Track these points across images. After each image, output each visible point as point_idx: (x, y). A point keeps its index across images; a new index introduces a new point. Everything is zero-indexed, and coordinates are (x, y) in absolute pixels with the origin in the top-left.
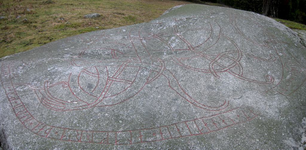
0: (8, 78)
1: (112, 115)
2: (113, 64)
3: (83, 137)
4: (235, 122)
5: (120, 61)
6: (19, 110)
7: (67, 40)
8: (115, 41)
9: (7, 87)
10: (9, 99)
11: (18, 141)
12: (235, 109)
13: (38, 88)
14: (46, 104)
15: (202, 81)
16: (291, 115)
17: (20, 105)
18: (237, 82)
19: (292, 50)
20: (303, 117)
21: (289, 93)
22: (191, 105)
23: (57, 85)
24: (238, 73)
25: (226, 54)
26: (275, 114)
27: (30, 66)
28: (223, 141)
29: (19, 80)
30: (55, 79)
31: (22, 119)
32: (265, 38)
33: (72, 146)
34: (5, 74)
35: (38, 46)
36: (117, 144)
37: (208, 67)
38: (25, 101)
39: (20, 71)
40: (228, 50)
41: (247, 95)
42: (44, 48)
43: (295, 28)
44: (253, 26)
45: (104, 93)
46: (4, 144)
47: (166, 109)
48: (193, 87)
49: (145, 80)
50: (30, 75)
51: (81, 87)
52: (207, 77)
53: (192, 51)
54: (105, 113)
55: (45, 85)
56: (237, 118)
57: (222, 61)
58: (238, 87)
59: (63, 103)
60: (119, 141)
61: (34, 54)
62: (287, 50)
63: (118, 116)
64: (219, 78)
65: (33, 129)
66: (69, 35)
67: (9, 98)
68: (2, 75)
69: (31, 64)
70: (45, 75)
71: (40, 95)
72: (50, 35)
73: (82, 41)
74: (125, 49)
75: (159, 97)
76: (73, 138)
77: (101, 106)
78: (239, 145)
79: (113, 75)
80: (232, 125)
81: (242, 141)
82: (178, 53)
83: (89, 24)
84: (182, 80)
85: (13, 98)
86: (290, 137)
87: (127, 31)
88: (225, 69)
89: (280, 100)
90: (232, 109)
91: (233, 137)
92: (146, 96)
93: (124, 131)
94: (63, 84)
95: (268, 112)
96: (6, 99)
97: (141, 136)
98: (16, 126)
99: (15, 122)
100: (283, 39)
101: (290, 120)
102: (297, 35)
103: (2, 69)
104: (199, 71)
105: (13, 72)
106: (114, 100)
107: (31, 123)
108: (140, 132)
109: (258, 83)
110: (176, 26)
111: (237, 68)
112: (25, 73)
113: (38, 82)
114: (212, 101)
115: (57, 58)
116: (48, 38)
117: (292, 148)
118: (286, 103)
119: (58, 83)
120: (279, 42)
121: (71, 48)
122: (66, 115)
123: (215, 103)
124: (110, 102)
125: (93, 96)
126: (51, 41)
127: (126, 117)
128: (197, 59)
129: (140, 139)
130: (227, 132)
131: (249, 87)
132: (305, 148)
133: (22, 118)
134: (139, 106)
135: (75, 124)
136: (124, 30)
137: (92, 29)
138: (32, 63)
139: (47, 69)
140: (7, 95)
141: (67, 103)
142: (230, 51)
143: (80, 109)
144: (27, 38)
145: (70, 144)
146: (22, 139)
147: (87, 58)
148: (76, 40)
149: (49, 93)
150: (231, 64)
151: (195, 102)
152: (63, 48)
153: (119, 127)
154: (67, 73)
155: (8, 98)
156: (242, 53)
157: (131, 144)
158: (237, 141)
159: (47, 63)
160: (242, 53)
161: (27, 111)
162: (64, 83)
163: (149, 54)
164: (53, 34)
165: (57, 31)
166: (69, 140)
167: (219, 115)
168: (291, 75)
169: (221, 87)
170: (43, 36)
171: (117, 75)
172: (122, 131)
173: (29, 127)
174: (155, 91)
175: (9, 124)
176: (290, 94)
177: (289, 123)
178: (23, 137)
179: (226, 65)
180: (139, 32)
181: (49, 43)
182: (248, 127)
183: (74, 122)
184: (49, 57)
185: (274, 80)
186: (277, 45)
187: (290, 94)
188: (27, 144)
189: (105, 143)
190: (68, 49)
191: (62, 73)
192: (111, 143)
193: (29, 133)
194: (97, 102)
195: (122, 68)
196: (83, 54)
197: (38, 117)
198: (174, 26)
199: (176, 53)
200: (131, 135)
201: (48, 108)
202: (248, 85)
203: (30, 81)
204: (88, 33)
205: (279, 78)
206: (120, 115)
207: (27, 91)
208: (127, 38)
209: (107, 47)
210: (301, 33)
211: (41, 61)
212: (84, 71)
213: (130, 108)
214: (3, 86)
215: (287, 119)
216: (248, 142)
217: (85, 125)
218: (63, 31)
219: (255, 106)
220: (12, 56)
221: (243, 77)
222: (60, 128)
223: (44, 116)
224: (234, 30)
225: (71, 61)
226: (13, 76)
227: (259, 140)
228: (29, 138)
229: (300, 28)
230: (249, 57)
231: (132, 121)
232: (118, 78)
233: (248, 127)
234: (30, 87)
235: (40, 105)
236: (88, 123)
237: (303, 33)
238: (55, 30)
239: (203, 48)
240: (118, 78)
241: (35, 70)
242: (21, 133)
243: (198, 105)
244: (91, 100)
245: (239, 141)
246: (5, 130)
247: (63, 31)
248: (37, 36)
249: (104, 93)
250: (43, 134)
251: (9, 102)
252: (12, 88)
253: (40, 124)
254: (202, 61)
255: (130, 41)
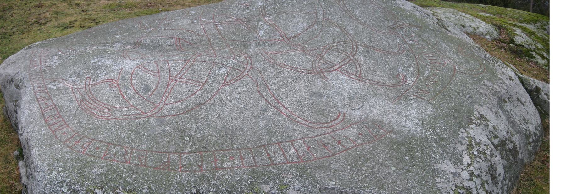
0: (38, 71)
1: (176, 129)
2: (176, 57)
3: (133, 158)
4: (357, 142)
5: (187, 53)
6: (50, 114)
7: (119, 25)
8: (180, 27)
9: (36, 83)
10: (37, 99)
11: (45, 155)
12: (355, 123)
13: (77, 86)
14: (86, 108)
15: (302, 86)
16: (440, 127)
17: (51, 107)
18: (353, 85)
19: (427, 35)
20: (460, 128)
21: (432, 95)
22: (287, 119)
23: (103, 83)
24: (355, 73)
25: (334, 46)
26: (415, 128)
27: (68, 56)
28: (342, 172)
29: (53, 74)
30: (100, 75)
31: (52, 126)
32: (389, 23)
33: (117, 169)
34: (34, 65)
35: (80, 30)
36: (183, 171)
37: (310, 66)
38: (59, 102)
39: (55, 62)
40: (336, 41)
41: (370, 103)
42: (89, 33)
43: (427, 6)
44: (369, 7)
45: (164, 98)
46: (28, 158)
47: (250, 125)
48: (289, 93)
49: (221, 80)
50: (67, 68)
51: (134, 89)
52: (309, 80)
53: (286, 43)
54: (165, 127)
55: (87, 83)
56: (359, 138)
57: (329, 57)
58: (356, 93)
59: (108, 109)
60: (185, 167)
61: (74, 40)
62: (419, 36)
63: (183, 131)
64: (327, 81)
65: (66, 141)
66: (122, 18)
67: (38, 97)
68: (31, 66)
69: (70, 54)
70: (88, 69)
71: (78, 95)
72: (96, 16)
73: (139, 26)
74: (194, 38)
75: (242, 106)
76: (119, 158)
77: (161, 117)
78: (366, 177)
79: (177, 73)
80: (353, 147)
81: (371, 171)
82: (266, 44)
83: (149, 5)
84: (273, 83)
85: (43, 98)
86: (445, 159)
87: (196, 13)
88: (334, 68)
89: (419, 106)
90: (350, 125)
91: (355, 165)
92: (223, 104)
93: (192, 153)
94: (110, 82)
95: (405, 126)
96: (33, 99)
97: (216, 160)
98: (44, 135)
99: (43, 130)
100: (411, 21)
101: (440, 134)
102: (431, 15)
103: (31, 58)
104: (297, 71)
105: (45, 63)
106: (177, 108)
107: (65, 133)
108: (214, 154)
109: (386, 86)
110: (263, 7)
111: (352, 66)
112: (60, 66)
113: (77, 78)
114: (321, 114)
115: (104, 48)
116: (94, 20)
117: (451, 175)
118: (430, 110)
119: (104, 81)
120: (405, 26)
121: (124, 34)
122: (112, 125)
123: (325, 116)
124: (173, 110)
125: (150, 102)
126: (97, 25)
127: (195, 132)
128: (294, 54)
129: (214, 165)
130: (347, 159)
131: (373, 91)
132: (470, 172)
133: (52, 125)
134: (213, 117)
135: (124, 139)
136: (193, 13)
137: (152, 12)
138: (71, 51)
139: (90, 61)
140: (35, 93)
141: (114, 109)
142: (339, 42)
143: (131, 119)
144: (66, 19)
145: (115, 166)
146: (51, 153)
147: (145, 49)
148: (130, 24)
149: (91, 93)
150: (343, 59)
151: (293, 115)
152: (113, 35)
153: (184, 147)
154: (116, 68)
155: (37, 97)
156: (356, 44)
157: (202, 171)
158: (363, 170)
159: (91, 53)
160: (356, 44)
161: (60, 116)
162: (112, 81)
163: (228, 44)
164: (100, 15)
165: (107, 12)
166: (114, 160)
167: (332, 134)
168: (431, 71)
169: (330, 93)
170: (87, 17)
171: (182, 74)
172: (189, 152)
173: (61, 138)
174: (236, 97)
175: (35, 132)
176: (434, 97)
177: (440, 138)
178: (52, 150)
179: (335, 61)
180: (213, 15)
181: (94, 27)
182: (378, 149)
183: (122, 136)
184: (94, 45)
185: (406, 79)
186: (404, 30)
187: (434, 97)
188: (57, 160)
189: (165, 169)
190: (120, 36)
191: (110, 67)
192: (173, 169)
193: (61, 145)
194: (155, 111)
195: (189, 64)
196: (139, 44)
197: (74, 125)
198: (261, 7)
199: (264, 45)
200: (202, 158)
201: (88, 113)
202: (371, 89)
203: (67, 76)
204: (147, 16)
205: (413, 75)
206: (187, 129)
207: (62, 90)
208: (197, 22)
209: (170, 35)
210: (437, 11)
211: (82, 49)
212: (139, 66)
213: (200, 120)
214: (31, 81)
215: (436, 133)
216: (379, 172)
217: (137, 141)
218: (114, 12)
219: (384, 118)
220: (45, 42)
221: (362, 78)
222: (103, 142)
223: (82, 125)
224: (342, 12)
225: (123, 52)
226: (45, 68)
227: (396, 168)
228: (60, 152)
229: (435, 4)
230: (368, 50)
231: (204, 138)
232: (183, 77)
233: (378, 149)
234: (66, 84)
235: (77, 109)
236: (141, 139)
237: (440, 12)
238: (104, 10)
239: (303, 40)
240: (183, 77)
241: (75, 62)
242: (51, 145)
243: (297, 119)
244: (147, 108)
245: (365, 171)
246: (29, 139)
247: (114, 12)
248: (80, 17)
249: (164, 98)
250: (79, 148)
251: (37, 103)
252: (42, 84)
253: (76, 135)
254: (302, 58)
255: (201, 27)
